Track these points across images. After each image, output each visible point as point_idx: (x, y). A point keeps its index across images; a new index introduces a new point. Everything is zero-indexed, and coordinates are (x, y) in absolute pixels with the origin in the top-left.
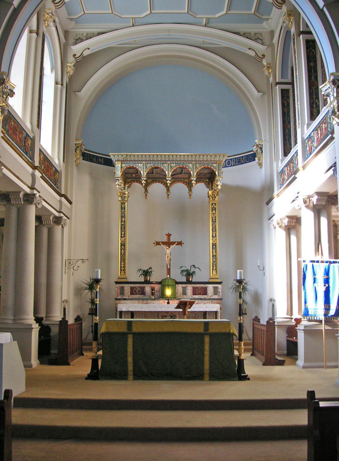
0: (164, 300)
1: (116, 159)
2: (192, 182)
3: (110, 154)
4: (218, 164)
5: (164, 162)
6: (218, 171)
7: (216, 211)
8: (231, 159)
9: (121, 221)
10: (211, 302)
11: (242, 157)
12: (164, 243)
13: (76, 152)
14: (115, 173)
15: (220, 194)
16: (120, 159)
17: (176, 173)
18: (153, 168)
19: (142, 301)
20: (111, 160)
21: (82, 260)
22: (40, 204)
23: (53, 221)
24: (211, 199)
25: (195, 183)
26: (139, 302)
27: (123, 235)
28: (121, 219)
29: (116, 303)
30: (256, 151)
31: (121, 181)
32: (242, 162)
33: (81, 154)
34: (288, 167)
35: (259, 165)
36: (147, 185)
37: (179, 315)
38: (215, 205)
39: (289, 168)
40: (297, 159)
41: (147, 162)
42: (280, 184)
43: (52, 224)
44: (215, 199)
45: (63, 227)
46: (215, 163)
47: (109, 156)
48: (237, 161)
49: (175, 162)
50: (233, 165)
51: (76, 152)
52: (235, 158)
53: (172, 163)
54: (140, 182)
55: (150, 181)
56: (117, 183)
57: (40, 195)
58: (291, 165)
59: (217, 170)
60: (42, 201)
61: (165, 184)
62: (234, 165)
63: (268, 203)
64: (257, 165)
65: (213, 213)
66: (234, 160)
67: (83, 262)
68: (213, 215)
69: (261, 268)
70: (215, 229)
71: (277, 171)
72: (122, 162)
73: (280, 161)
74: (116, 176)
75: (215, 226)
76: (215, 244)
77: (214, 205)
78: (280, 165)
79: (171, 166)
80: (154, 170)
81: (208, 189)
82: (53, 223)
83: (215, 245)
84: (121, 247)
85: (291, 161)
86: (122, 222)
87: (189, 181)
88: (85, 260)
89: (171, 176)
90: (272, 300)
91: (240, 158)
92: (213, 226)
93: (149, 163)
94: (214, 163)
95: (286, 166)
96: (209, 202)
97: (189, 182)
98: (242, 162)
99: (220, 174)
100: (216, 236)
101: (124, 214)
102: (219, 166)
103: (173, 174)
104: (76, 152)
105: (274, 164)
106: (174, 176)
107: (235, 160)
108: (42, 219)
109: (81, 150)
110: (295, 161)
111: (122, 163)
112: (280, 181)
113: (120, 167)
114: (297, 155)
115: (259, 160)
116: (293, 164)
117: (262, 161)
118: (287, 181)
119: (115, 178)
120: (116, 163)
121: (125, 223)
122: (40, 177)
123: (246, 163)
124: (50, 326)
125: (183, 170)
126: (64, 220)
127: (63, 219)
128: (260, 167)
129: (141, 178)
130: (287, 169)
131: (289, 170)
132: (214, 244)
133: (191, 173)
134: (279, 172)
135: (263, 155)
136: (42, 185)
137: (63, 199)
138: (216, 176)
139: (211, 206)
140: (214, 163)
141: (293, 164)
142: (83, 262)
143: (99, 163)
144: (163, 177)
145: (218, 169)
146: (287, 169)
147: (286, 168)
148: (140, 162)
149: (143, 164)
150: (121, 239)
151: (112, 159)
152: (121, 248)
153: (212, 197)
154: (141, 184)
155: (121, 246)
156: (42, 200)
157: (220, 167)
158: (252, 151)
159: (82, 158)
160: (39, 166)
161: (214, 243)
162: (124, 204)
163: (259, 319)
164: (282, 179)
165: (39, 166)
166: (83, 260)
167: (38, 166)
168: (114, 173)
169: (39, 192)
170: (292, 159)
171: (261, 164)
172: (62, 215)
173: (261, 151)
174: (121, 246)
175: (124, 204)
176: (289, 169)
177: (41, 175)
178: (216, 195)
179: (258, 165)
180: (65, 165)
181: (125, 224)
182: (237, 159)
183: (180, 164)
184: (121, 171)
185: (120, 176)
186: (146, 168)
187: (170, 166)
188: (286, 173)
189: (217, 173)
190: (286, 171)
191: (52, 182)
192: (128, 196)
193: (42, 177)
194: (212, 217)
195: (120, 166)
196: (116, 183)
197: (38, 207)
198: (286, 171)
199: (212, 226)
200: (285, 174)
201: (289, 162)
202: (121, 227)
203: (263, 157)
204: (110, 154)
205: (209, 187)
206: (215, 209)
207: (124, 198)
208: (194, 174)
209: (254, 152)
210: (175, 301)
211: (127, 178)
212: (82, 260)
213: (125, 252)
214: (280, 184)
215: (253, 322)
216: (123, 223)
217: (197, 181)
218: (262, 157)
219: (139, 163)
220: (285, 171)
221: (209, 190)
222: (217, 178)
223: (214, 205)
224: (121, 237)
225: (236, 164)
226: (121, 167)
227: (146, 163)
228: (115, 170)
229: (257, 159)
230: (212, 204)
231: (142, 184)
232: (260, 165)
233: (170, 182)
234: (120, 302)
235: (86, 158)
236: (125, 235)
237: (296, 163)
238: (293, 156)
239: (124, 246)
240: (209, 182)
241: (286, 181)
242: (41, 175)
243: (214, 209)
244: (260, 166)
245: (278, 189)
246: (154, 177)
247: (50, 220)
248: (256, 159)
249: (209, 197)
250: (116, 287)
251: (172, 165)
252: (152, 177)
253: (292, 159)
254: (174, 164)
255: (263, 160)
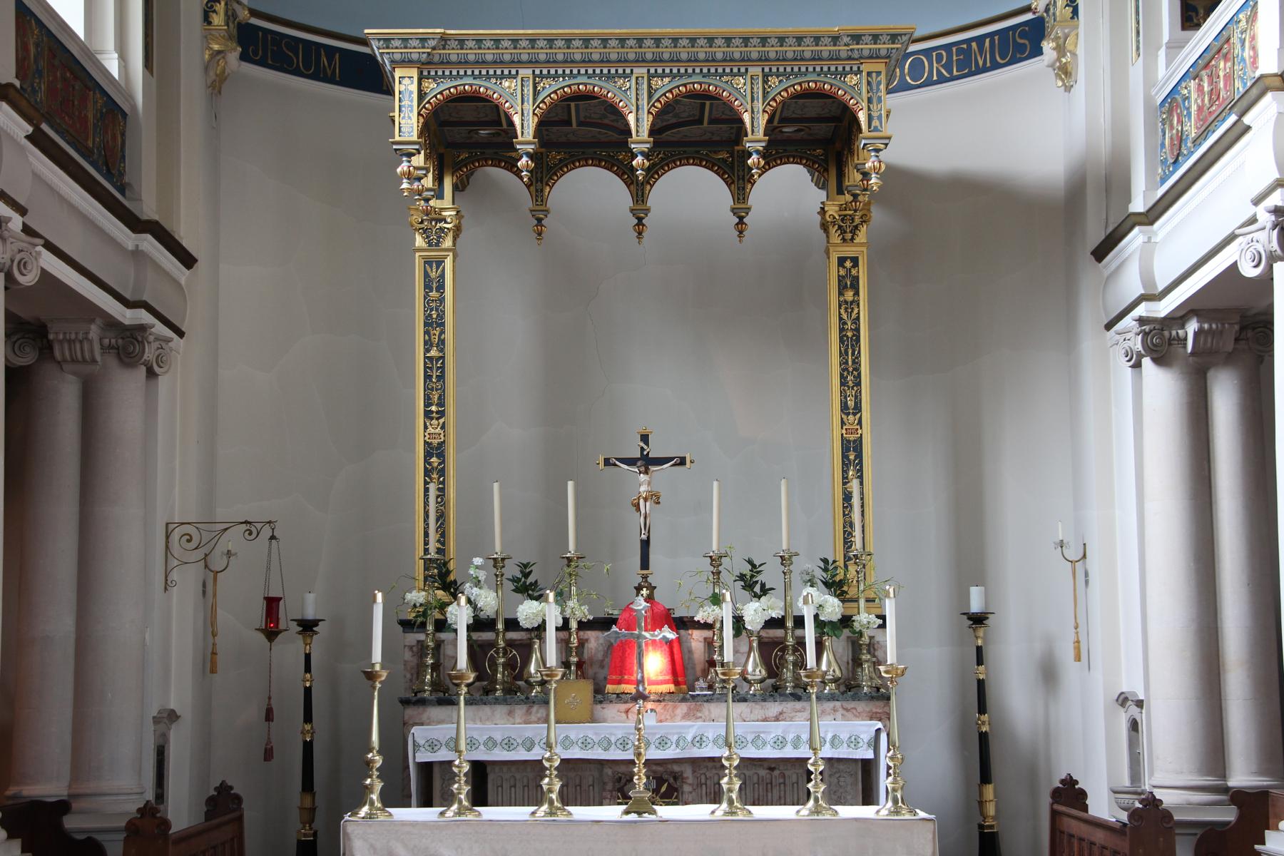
0: (626, 702)
1: (397, 57)
2: (750, 162)
3: (366, 31)
4: (869, 74)
5: (620, 65)
6: (869, 109)
7: (857, 293)
8: (927, 52)
9: (426, 343)
10: (841, 711)
11: (980, 40)
12: (630, 462)
13: (207, 19)
14: (393, 121)
15: (876, 214)
16: (415, 57)
17: (673, 121)
18: (567, 99)
19: (525, 707)
20: (372, 58)
21: (244, 527)
22: (29, 267)
23: (102, 346)
24: (835, 238)
25: (762, 162)
26: (510, 713)
27: (434, 408)
28: (426, 332)
29: (406, 718)
30: (1047, 10)
31: (419, 160)
32: (981, 63)
33: (235, 32)
34: (1201, 80)
35: (1057, 75)
36: (544, 174)
37: (694, 772)
38: (854, 266)
39: (1211, 83)
40: (1253, 38)
41: (537, 72)
42: (1164, 162)
43: (98, 358)
44: (852, 239)
45: (151, 374)
46: (855, 68)
47: (364, 42)
48: (955, 58)
49: (667, 71)
50: (935, 78)
51: (210, 23)
52: (947, 47)
53: (656, 75)
54: (511, 166)
55: (555, 156)
56: (403, 167)
57: (26, 222)
58: (1217, 67)
59: (864, 104)
60: (39, 253)
61: (625, 172)
62: (942, 80)
63: (1100, 253)
64: (1051, 73)
65: (846, 302)
66: (939, 58)
67: (250, 534)
68: (846, 309)
69: (1073, 553)
70: (855, 373)
71: (1148, 100)
72: (426, 68)
73: (1162, 53)
74: (397, 138)
75: (854, 362)
76: (855, 441)
77: (848, 264)
78: (1162, 71)
79: (650, 86)
80: (573, 104)
81: (822, 195)
82: (103, 354)
83: (857, 446)
84: (425, 461)
85: (1220, 47)
86: (432, 346)
87: (732, 156)
88: (259, 526)
89: (651, 133)
90: (1126, 699)
91: (970, 47)
92: (847, 363)
93: (549, 76)
94: (848, 69)
95: (1193, 73)
96: (827, 252)
97: (732, 162)
98: (981, 63)
99: (875, 123)
100: (858, 408)
101: (437, 310)
102: (874, 87)
103: (660, 125)
104: (207, 19)
105: (1131, 69)
106: (665, 136)
107: (944, 53)
108: (51, 337)
109: (230, 16)
110: (1243, 50)
111: (425, 73)
112: (1163, 145)
113: (415, 96)
114: (1252, 19)
115: (1061, 50)
116: (1229, 64)
117: (1074, 55)
118: (1200, 144)
119: (395, 147)
120: (398, 73)
121: (442, 350)
122: (28, 137)
123: (996, 66)
124: (99, 837)
125: (708, 103)
126: (157, 339)
127: (151, 338)
128: (1064, 84)
129: (511, 147)
130: (1200, 88)
131: (1211, 92)
132: (849, 441)
133: (741, 121)
134: (1158, 104)
135: (1077, 27)
136: (37, 177)
137: (148, 243)
138: (860, 130)
139: (834, 272)
140: (848, 69)
141: (1229, 64)
142: (250, 534)
143: (319, 75)
144: (615, 137)
145: (870, 100)
146: (1200, 88)
147: (1193, 84)
148: (506, 72)
149: (519, 79)
150: (426, 427)
151: (379, 58)
152: (425, 468)
153: (840, 227)
154: (514, 173)
155: (425, 457)
156: (40, 248)
157: (878, 89)
158: (1027, 9)
159: (240, 49)
160: (17, 83)
161: (852, 437)
162: (440, 263)
163: (1083, 794)
164: (1171, 138)
165: (17, 83)
166: (250, 523)
167: (10, 85)
168: (391, 123)
169: (22, 211)
170: (1223, 38)
171: (1069, 69)
172: (144, 317)
173: (1070, 9)
174: (428, 455)
175: (437, 268)
176: (1206, 89)
177: (30, 129)
178: (857, 220)
179: (1053, 76)
180: (154, 81)
181: (443, 358)
182: (954, 49)
183: (690, 76)
184: (419, 114)
185: (415, 138)
186: (535, 99)
187: (645, 86)
188: (1194, 108)
189: (862, 116)
190: (1194, 96)
191: (92, 164)
192: (457, 230)
193: (37, 139)
194: (841, 319)
195: (414, 88)
196: (399, 170)
197: (19, 284)
198: (1194, 96)
199: (844, 363)
200: (1189, 114)
201: (1208, 56)
202: (425, 372)
203: (1077, 35)
204: (366, 31)
205: (826, 180)
206: (856, 279)
207: (440, 237)
208: (755, 123)
209: (1034, 13)
210: (675, 707)
211: (453, 145)
212: (246, 522)
213: (443, 483)
214: (1164, 162)
215: (1052, 804)
216: (434, 353)
217: (777, 153)
218: (1073, 34)
219: (502, 77)
220: (1188, 98)
221: (824, 199)
222: (863, 142)
223: (848, 264)
224: (428, 414)
225: (950, 72)
226: (421, 95)
227: (535, 76)
228: (393, 111)
229: (1052, 45)
230: (841, 261)
231: (518, 173)
232: (1065, 72)
233: (647, 164)
234: (424, 717)
235: (256, 53)
236: (443, 405)
237: (1243, 60)
238: (1233, 20)
239: (441, 456)
240: (826, 161)
241: (1189, 144)
242: (30, 129)
243: (848, 283)
244: (1063, 80)
245: (1150, 187)
246: (572, 138)
247: (91, 342)
248: (1047, 46)
249: (825, 227)
250: (405, 646)
251: (653, 82)
252: (563, 139)
253: (1223, 39)
254: (666, 80)
255: (1080, 51)
